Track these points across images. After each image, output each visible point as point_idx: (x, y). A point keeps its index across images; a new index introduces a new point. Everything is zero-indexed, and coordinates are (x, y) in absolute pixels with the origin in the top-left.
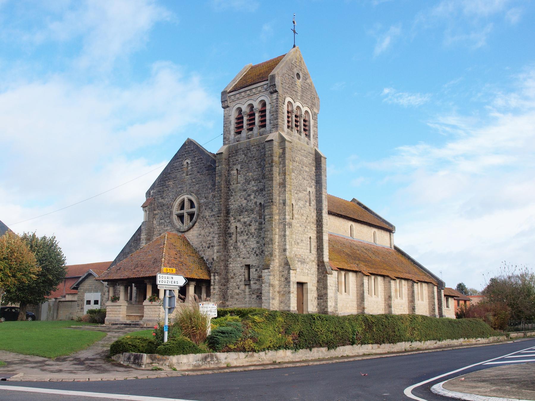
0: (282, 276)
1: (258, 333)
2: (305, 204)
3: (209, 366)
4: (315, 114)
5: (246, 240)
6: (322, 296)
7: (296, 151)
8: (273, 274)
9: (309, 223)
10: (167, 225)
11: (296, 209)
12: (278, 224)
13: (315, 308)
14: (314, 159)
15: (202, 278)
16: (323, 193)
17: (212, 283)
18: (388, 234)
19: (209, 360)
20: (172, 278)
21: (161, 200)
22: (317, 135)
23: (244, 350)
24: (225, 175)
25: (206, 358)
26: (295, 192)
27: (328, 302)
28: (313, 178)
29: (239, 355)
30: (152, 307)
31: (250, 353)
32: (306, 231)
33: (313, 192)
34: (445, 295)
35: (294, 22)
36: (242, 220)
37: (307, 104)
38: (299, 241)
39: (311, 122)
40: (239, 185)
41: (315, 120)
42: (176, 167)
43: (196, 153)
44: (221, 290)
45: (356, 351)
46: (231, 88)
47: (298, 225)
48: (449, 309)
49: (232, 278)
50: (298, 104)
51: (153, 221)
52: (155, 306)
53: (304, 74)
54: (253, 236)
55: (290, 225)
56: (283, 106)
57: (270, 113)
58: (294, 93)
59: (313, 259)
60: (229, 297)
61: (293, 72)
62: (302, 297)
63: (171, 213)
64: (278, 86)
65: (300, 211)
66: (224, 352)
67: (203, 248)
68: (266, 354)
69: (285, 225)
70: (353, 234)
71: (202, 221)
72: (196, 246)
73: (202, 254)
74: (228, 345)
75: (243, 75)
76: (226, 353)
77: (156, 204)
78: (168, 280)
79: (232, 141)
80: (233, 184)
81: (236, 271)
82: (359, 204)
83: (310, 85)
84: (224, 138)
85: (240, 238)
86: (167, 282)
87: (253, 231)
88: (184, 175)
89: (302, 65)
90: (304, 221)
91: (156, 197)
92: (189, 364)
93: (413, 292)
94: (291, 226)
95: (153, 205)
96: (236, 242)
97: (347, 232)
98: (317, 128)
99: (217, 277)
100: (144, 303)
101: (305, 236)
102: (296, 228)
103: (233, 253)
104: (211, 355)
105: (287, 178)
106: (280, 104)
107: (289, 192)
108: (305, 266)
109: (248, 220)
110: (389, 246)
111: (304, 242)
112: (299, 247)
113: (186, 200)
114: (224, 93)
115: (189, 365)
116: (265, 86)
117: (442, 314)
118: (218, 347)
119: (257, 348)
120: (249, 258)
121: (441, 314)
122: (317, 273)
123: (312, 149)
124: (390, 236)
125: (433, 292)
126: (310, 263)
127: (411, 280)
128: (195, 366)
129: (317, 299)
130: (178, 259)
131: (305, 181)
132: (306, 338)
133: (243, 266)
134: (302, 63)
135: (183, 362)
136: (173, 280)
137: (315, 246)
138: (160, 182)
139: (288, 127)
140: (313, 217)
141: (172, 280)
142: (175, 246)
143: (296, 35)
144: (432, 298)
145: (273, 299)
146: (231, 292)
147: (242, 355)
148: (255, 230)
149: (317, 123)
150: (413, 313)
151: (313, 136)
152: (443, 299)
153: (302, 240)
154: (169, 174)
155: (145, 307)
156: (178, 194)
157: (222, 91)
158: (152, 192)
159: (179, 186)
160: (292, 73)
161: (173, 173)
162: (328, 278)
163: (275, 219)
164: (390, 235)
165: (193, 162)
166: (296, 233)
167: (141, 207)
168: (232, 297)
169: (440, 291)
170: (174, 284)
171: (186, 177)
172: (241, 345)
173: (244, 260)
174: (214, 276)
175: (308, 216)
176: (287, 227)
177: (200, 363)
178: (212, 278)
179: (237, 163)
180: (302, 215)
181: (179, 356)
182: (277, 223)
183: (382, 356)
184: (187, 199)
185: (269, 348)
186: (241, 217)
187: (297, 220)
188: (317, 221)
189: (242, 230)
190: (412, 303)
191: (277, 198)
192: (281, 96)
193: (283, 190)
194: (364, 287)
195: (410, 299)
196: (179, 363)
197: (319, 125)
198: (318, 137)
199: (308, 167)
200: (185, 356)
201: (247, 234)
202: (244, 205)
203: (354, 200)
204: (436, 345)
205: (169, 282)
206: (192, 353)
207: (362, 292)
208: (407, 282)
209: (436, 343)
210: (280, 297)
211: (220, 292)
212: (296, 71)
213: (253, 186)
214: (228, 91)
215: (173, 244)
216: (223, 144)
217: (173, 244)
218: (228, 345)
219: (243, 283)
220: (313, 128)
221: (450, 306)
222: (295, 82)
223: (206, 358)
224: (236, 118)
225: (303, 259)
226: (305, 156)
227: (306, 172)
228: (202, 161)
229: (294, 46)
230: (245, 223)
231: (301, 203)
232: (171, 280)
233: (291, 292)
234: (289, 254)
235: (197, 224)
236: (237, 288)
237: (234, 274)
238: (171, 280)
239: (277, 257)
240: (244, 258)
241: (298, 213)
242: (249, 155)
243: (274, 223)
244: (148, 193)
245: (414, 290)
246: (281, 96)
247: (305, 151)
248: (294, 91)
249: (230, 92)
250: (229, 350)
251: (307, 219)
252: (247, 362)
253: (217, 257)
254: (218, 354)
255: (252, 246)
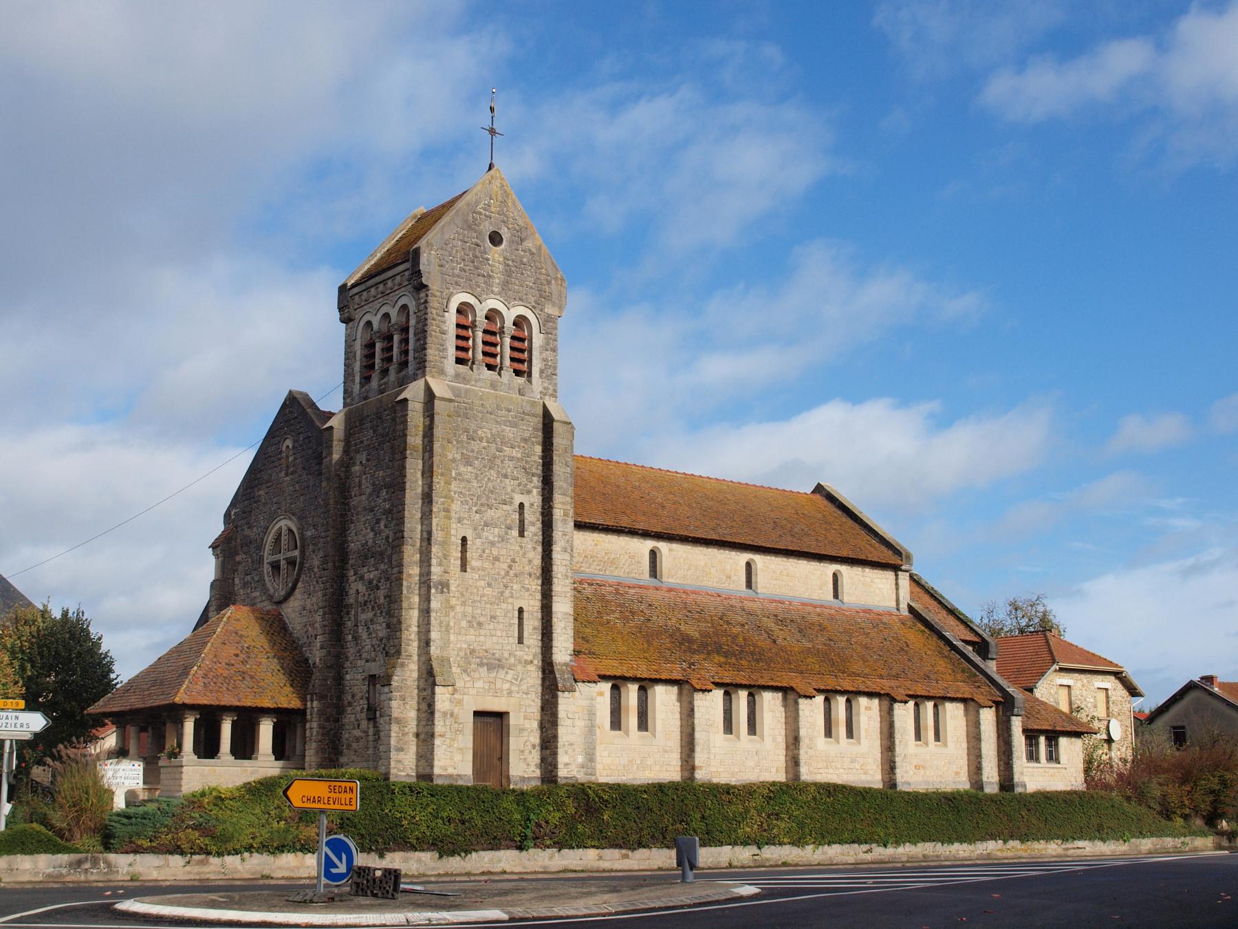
0: (423, 699)
1: (217, 819)
2: (506, 534)
3: (86, 877)
4: (549, 324)
5: (371, 620)
6: (549, 743)
7: (480, 415)
8: (401, 696)
9: (516, 575)
10: (255, 588)
11: (474, 547)
12: (418, 586)
13: (533, 768)
14: (540, 426)
15: (285, 706)
16: (556, 506)
17: (309, 717)
18: (890, 575)
19: (87, 865)
20: (17, 718)
21: (247, 532)
22: (555, 368)
23: (177, 850)
24: (339, 475)
25: (79, 863)
26: (474, 509)
27: (559, 756)
28: (534, 471)
29: (167, 860)
30: (170, 770)
31: (196, 857)
32: (507, 593)
33: (532, 505)
34: (1025, 731)
35: (492, 109)
36: (366, 576)
37: (521, 300)
38: (482, 619)
39: (533, 340)
40: (363, 497)
41: (547, 333)
42: (271, 457)
43: (301, 425)
44: (325, 731)
45: (540, 863)
46: (359, 275)
47: (482, 583)
48: (1058, 766)
49: (350, 704)
50: (493, 303)
51: (234, 578)
52: (175, 769)
53: (515, 229)
54: (381, 613)
55: (444, 586)
56: (443, 316)
57: (415, 334)
58: (481, 279)
59: (530, 658)
60: (345, 747)
61: (480, 234)
62: (498, 745)
63: (261, 560)
64: (429, 273)
65: (487, 551)
66: (127, 853)
67: (308, 637)
68: (243, 860)
69: (429, 587)
70: (756, 583)
71: (308, 579)
72: (298, 635)
73: (306, 651)
74: (133, 839)
75: (396, 239)
76: (132, 855)
77: (238, 540)
78: (7, 721)
79: (357, 399)
80: (355, 495)
81: (355, 689)
82: (831, 498)
83: (532, 254)
84: (345, 391)
85: (363, 617)
86: (4, 725)
87: (382, 600)
88: (283, 474)
89: (508, 211)
90: (503, 573)
91: (239, 523)
92: (36, 873)
93: (891, 725)
94: (448, 589)
95: (233, 543)
96: (357, 626)
97: (734, 578)
98: (554, 350)
99: (315, 703)
100: (161, 763)
101: (504, 606)
102: (475, 591)
103: (351, 651)
104: (92, 857)
105: (438, 483)
106: (433, 312)
107: (443, 514)
108: (502, 673)
109: (375, 575)
110: (894, 604)
111: (500, 621)
112: (482, 632)
113: (284, 531)
114: (343, 289)
115: (37, 874)
116: (407, 273)
117: (1012, 779)
118: (112, 844)
119: (215, 848)
120: (375, 660)
121: (1007, 783)
122: (540, 689)
123: (533, 404)
124: (897, 579)
125: (977, 724)
126: (519, 668)
127: (888, 695)
128: (49, 875)
129: (538, 748)
130: (237, 666)
131: (507, 481)
132: (363, 832)
133: (365, 678)
134: (510, 204)
135: (20, 868)
136: (19, 722)
137: (534, 628)
138: (246, 489)
139: (459, 361)
140: (530, 561)
141: (16, 721)
142: (241, 636)
143: (497, 139)
144: (974, 738)
145: (400, 750)
146: (347, 736)
147: (176, 861)
148: (385, 597)
149: (556, 340)
150: (890, 778)
151: (542, 371)
152: (1019, 740)
153: (493, 617)
154: (260, 471)
155: (570, 766)
156: (272, 518)
157: (339, 285)
158: (233, 513)
159: (275, 500)
160: (475, 235)
161: (266, 469)
162: (560, 701)
163: (410, 576)
164: (897, 576)
165: (296, 445)
166: (474, 602)
167: (210, 547)
168: (349, 746)
169: (1008, 722)
170: (22, 729)
171: (285, 479)
172: (170, 842)
173: (368, 664)
174: (312, 700)
175: (513, 561)
176: (433, 591)
177: (64, 871)
178: (309, 704)
179: (361, 449)
180: (497, 559)
181: (12, 856)
182: (416, 584)
183: (591, 874)
184: (286, 528)
185: (249, 849)
186: (365, 569)
187: (480, 572)
188: (543, 569)
189: (366, 598)
190: (890, 753)
191: (416, 528)
192: (438, 294)
193: (428, 509)
194: (694, 718)
195: (886, 743)
196: (12, 870)
197: (560, 344)
198: (558, 371)
199: (519, 447)
200: (27, 857)
201: (373, 608)
202: (370, 542)
203: (819, 489)
204: (869, 857)
205: (9, 725)
206: (46, 852)
207: (689, 730)
208: (880, 700)
209: (870, 850)
210: (418, 746)
211: (323, 735)
212: (487, 228)
213: (384, 501)
214: (349, 284)
215: (237, 633)
216: (344, 403)
217: (237, 633)
218: (133, 839)
219: (364, 715)
220: (541, 353)
221: (1063, 757)
222: (485, 253)
223: (79, 863)
224: (365, 346)
225: (495, 659)
226: (508, 424)
227: (511, 459)
228: (310, 442)
229: (491, 167)
230: (370, 582)
231: (491, 534)
232: (14, 721)
233: (436, 734)
234: (438, 652)
235: (300, 585)
236: (356, 727)
237: (353, 696)
238: (14, 721)
239: (415, 658)
240: (367, 661)
241: (481, 556)
242: (380, 430)
243: (405, 583)
244: (227, 515)
245: (893, 721)
246: (438, 294)
247: (509, 411)
248: (479, 275)
249: (353, 286)
250: (137, 850)
251: (510, 567)
252: (189, 873)
253: (320, 660)
254: (112, 857)
255: (381, 634)
